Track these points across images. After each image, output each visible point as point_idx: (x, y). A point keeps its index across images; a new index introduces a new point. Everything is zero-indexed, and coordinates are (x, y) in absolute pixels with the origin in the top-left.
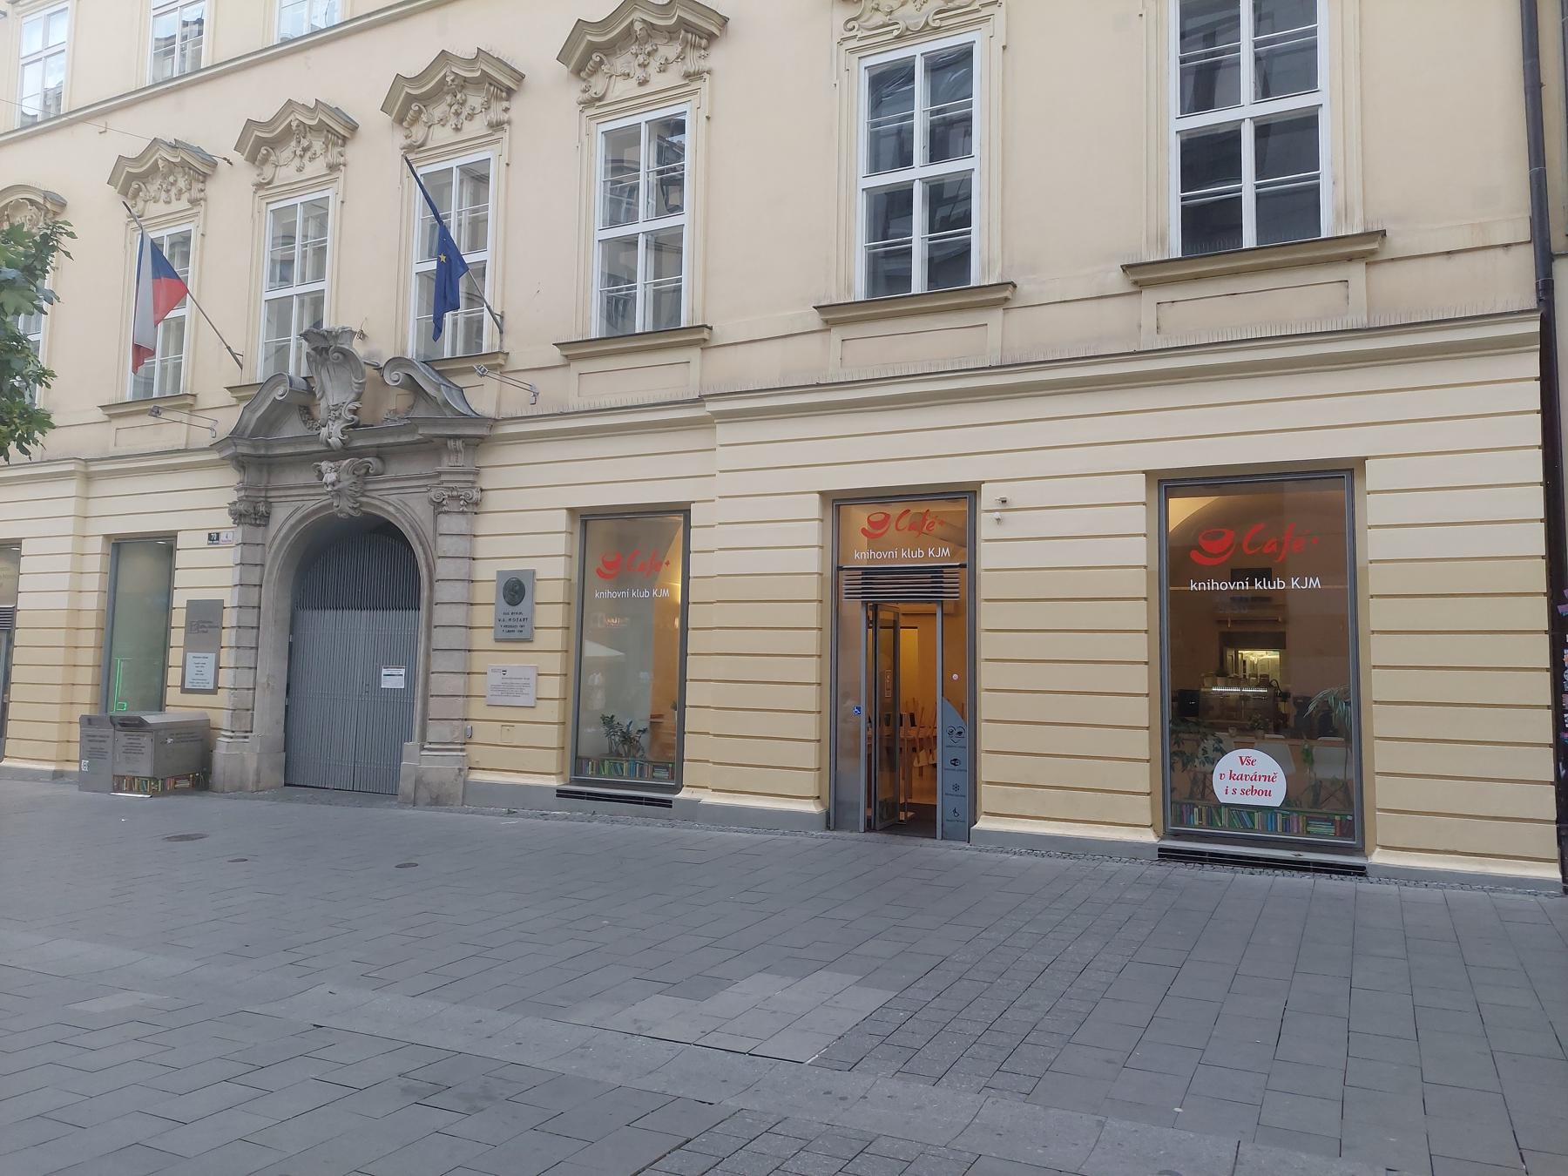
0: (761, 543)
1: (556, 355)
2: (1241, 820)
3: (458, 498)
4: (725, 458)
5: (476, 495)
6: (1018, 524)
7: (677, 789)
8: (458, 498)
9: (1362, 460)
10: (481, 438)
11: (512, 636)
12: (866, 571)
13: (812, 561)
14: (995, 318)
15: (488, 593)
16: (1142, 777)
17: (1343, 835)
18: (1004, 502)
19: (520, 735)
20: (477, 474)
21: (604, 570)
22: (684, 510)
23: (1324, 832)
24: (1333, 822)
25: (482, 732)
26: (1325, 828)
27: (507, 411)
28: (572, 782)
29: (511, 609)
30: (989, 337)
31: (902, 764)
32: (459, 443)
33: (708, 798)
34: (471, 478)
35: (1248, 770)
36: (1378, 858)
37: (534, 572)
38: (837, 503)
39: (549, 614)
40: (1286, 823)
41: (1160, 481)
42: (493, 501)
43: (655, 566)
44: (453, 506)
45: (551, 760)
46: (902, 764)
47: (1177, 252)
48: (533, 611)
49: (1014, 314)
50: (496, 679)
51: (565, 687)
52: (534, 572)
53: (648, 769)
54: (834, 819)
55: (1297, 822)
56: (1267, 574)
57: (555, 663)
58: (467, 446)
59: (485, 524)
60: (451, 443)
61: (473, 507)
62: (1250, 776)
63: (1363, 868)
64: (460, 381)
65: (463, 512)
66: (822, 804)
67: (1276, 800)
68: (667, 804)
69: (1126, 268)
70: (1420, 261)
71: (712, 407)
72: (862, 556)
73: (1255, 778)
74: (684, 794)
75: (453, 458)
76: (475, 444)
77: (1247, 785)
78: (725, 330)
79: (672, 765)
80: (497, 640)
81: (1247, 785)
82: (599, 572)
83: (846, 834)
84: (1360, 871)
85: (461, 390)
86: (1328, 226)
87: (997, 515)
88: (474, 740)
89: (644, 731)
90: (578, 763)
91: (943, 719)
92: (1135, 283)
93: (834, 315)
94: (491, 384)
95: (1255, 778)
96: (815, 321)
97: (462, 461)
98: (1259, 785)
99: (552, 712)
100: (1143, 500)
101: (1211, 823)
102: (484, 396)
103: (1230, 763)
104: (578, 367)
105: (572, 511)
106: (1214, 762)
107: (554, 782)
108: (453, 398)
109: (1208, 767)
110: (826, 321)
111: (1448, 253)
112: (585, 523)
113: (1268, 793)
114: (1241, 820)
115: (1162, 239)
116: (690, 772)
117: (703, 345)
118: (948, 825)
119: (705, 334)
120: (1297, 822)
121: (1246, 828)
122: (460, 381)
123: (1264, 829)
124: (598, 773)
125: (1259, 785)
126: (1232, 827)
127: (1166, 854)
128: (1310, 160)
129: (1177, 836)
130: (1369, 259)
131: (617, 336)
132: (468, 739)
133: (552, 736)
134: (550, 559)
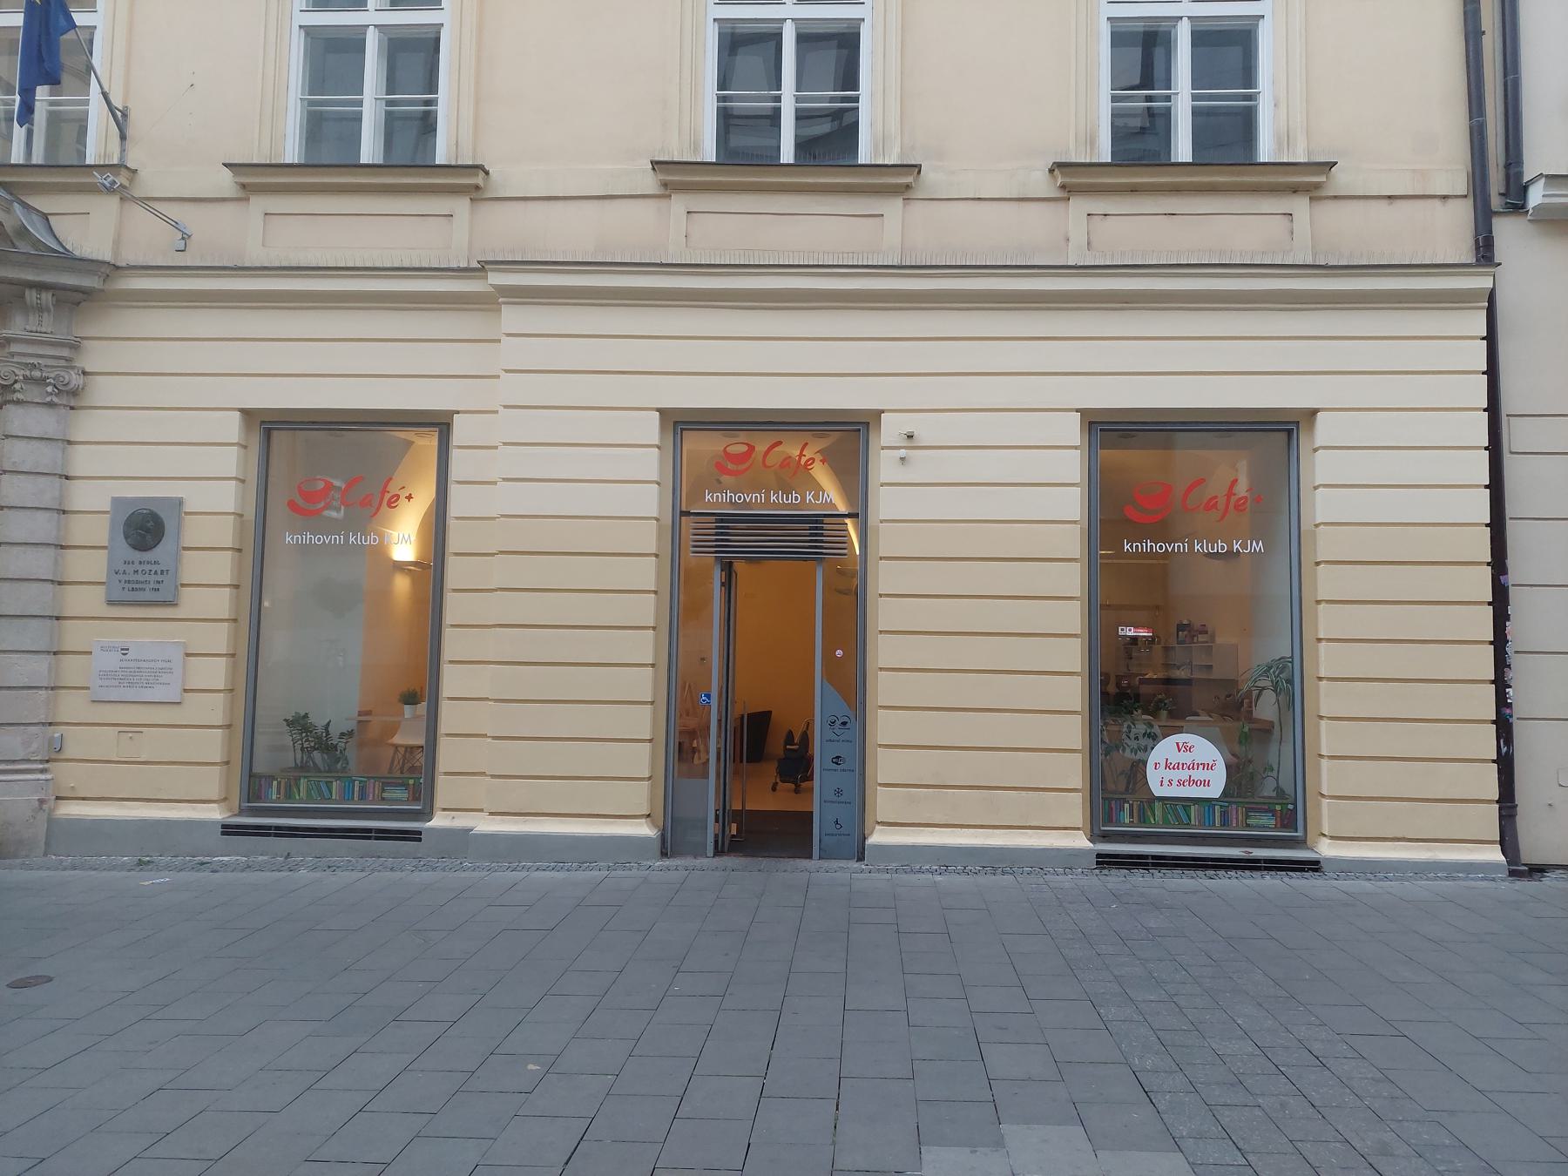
0: (554, 479)
1: (226, 182)
2: (1178, 817)
3: (42, 381)
4: (513, 353)
5: (75, 380)
6: (924, 466)
7: (427, 814)
8: (42, 381)
9: (1313, 413)
10: (87, 293)
11: (140, 596)
12: (722, 518)
13: (649, 502)
14: (892, 208)
15: (94, 528)
16: (1073, 772)
17: (1284, 826)
18: (910, 437)
19: (150, 745)
20: (75, 346)
21: (300, 502)
22: (440, 424)
23: (1265, 824)
24: (1274, 813)
25: (78, 743)
26: (1267, 820)
27: (129, 257)
28: (242, 812)
29: (138, 556)
30: (891, 229)
31: (763, 761)
32: (47, 297)
33: (485, 825)
34: (65, 353)
35: (1185, 758)
36: (1326, 849)
37: (180, 502)
38: (680, 424)
39: (207, 567)
40: (1224, 814)
41: (676, 423)
42: (103, 391)
43: (375, 501)
44: (33, 393)
45: (211, 782)
46: (763, 761)
47: (1106, 157)
48: (177, 560)
49: (917, 208)
50: (112, 661)
51: (233, 671)
52: (180, 502)
53: (373, 788)
54: (667, 847)
55: (1237, 814)
56: (1162, 532)
57: (219, 638)
58: (59, 303)
59: (87, 426)
60: (31, 296)
61: (69, 397)
62: (1187, 764)
63: (1317, 862)
64: (41, 203)
65: (51, 405)
66: (654, 824)
67: (1215, 789)
68: (414, 836)
69: (656, 164)
70: (521, 204)
71: (497, 279)
72: (716, 500)
73: (1192, 767)
74: (439, 821)
75: (33, 320)
76: (74, 301)
77: (1183, 774)
78: (507, 175)
79: (416, 776)
80: (111, 603)
81: (1183, 774)
82: (292, 505)
83: (689, 861)
84: (1314, 866)
85: (45, 217)
86: (1266, 150)
87: (903, 452)
88: (67, 754)
89: (350, 734)
90: (253, 787)
91: (823, 703)
92: (1063, 187)
93: (675, 176)
94: (104, 210)
95: (1192, 767)
96: (648, 182)
97: (48, 325)
98: (1198, 774)
99: (214, 709)
100: (657, 442)
101: (1143, 820)
102: (88, 228)
103: (1165, 750)
104: (260, 203)
105: (247, 414)
106: (1147, 750)
107: (215, 814)
108: (32, 223)
109: (1140, 755)
110: (665, 185)
111: (1389, 197)
112: (268, 434)
113: (1206, 783)
114: (1178, 817)
115: (1092, 141)
116: (445, 789)
117: (475, 193)
118: (826, 839)
119: (479, 179)
120: (1237, 814)
121: (1181, 824)
122: (41, 203)
123: (1202, 825)
124: (289, 796)
125: (1198, 774)
126: (1166, 823)
127: (1106, 861)
128: (1248, 76)
129: (1106, 837)
130: (1313, 192)
131: (327, 161)
132: (54, 754)
133: (213, 746)
134: (210, 488)
